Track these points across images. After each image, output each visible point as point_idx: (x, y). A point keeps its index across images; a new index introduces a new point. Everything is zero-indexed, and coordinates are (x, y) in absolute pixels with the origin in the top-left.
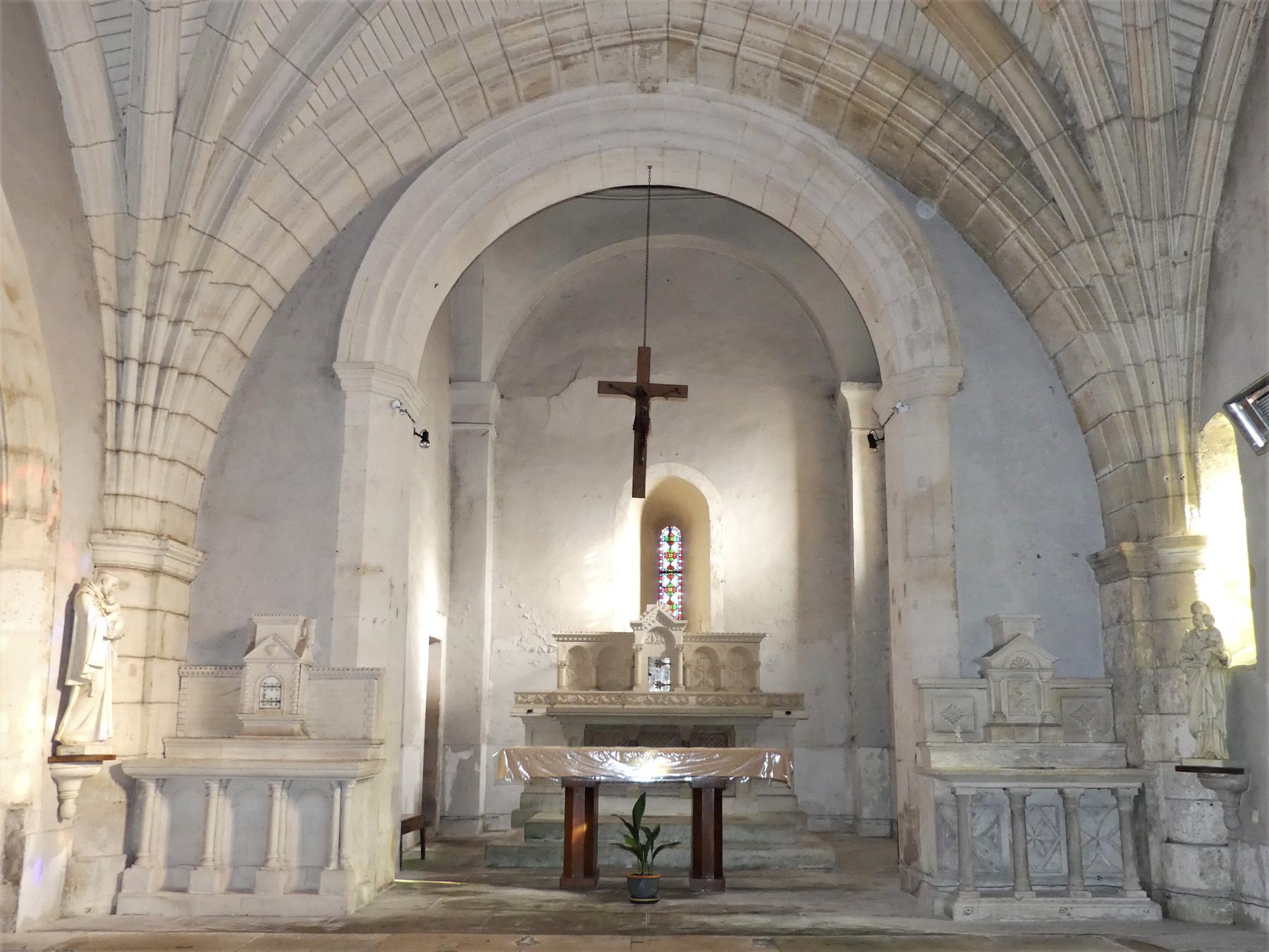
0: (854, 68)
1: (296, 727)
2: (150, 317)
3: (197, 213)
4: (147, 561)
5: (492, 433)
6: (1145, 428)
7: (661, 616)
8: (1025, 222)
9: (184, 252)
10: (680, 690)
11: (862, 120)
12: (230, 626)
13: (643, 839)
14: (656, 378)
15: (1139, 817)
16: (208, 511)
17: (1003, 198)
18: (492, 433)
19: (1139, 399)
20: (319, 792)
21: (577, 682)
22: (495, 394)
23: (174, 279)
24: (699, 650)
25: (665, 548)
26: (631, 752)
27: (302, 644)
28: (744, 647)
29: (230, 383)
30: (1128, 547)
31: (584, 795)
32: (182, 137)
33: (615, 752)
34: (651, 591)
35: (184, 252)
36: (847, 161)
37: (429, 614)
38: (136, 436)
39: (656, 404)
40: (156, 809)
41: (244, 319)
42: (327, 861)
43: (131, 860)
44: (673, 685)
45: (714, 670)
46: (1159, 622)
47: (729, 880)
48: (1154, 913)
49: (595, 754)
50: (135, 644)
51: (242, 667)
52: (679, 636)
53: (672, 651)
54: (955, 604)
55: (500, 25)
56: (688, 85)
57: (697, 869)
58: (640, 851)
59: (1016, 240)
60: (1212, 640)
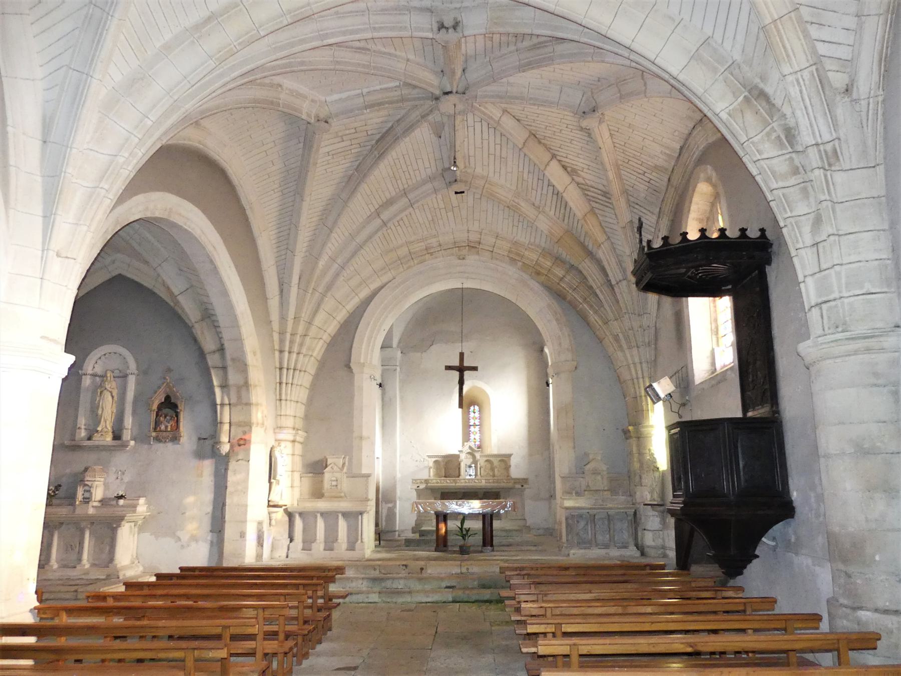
0: (534, 256)
1: (342, 494)
2: (290, 352)
3: (305, 316)
4: (292, 438)
5: (398, 369)
6: (637, 387)
7: (470, 447)
8: (596, 312)
9: (301, 329)
10: (479, 477)
11: (538, 273)
12: (317, 459)
13: (464, 532)
14: (466, 364)
15: (635, 519)
16: (307, 417)
17: (587, 303)
18: (398, 369)
19: (635, 376)
20: (353, 517)
21: (438, 475)
22: (399, 352)
23: (298, 339)
24: (486, 461)
25: (472, 415)
26: (460, 502)
27: (344, 464)
28: (505, 459)
29: (313, 372)
30: (631, 428)
31: (442, 517)
32: (301, 291)
33: (454, 502)
34: (466, 437)
35: (301, 329)
36: (534, 284)
37: (378, 451)
38: (286, 394)
39: (466, 373)
40: (298, 523)
41: (318, 349)
42: (357, 540)
43: (291, 541)
44: (476, 475)
45: (492, 469)
46: (641, 454)
47: (495, 548)
48: (638, 554)
49: (447, 503)
50: (289, 468)
51: (323, 473)
52: (478, 455)
53: (475, 462)
54: (574, 448)
55: (408, 243)
56: (477, 257)
57: (485, 544)
58: (464, 537)
59: (593, 317)
60: (654, 461)
